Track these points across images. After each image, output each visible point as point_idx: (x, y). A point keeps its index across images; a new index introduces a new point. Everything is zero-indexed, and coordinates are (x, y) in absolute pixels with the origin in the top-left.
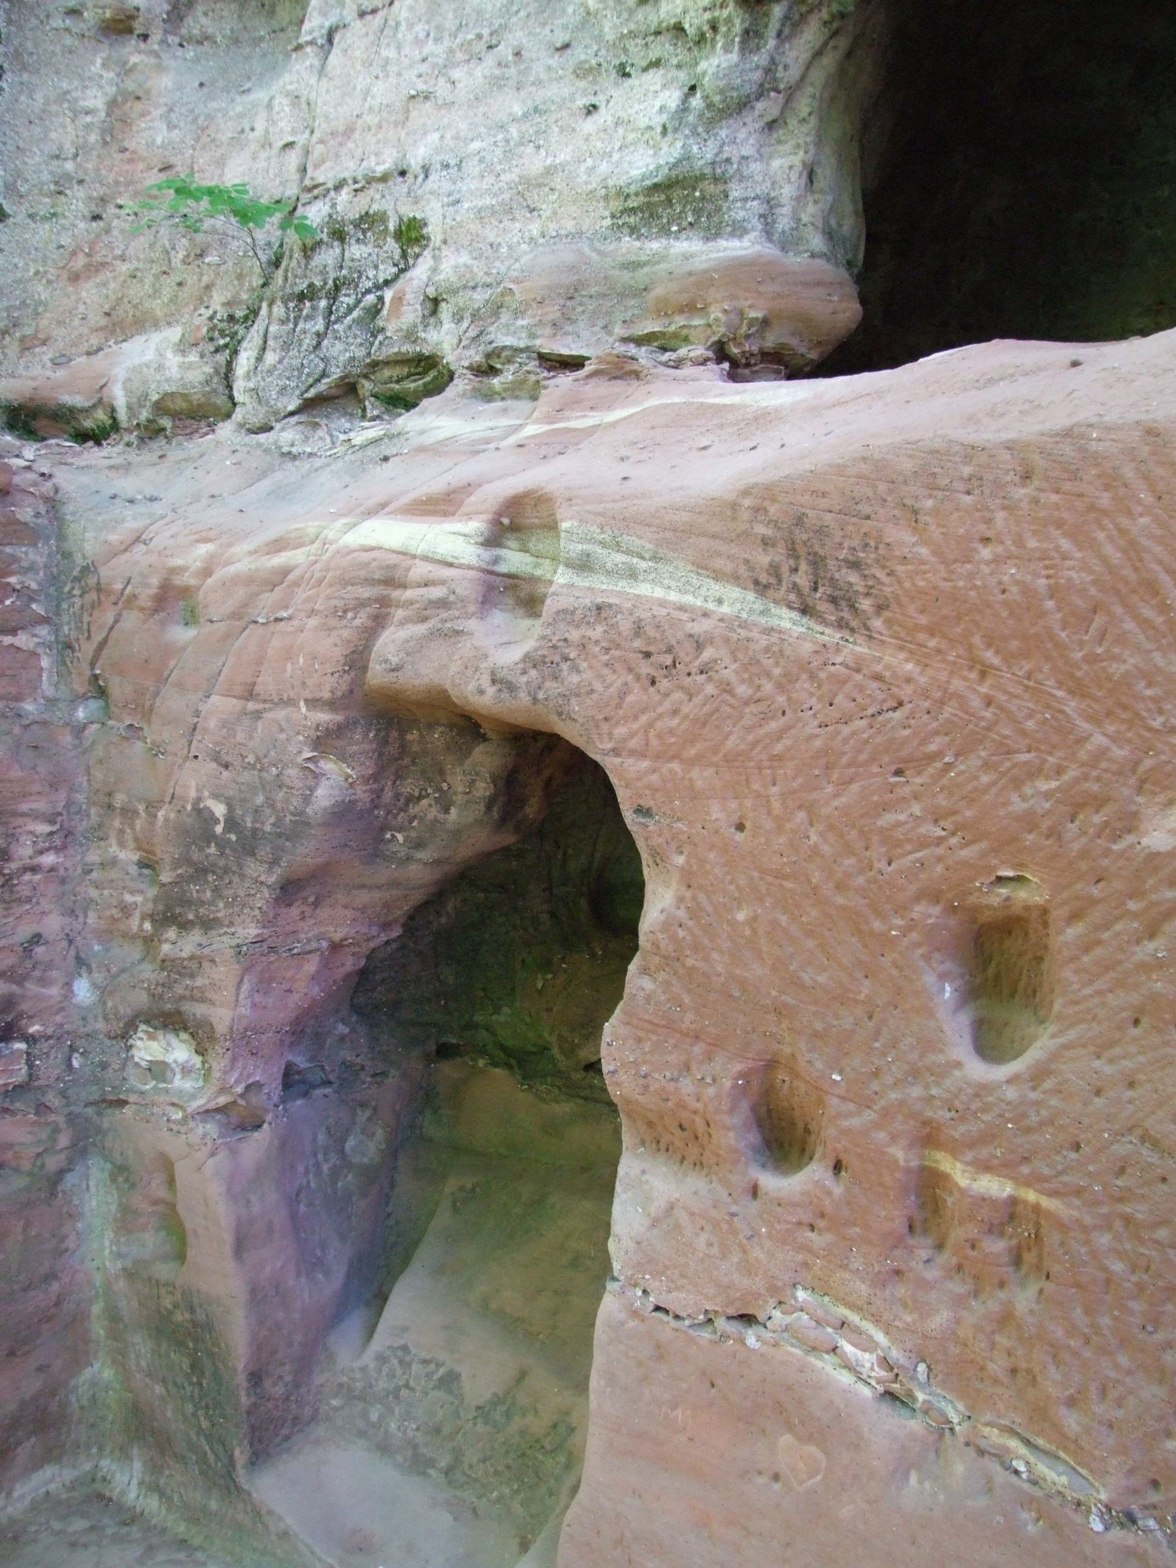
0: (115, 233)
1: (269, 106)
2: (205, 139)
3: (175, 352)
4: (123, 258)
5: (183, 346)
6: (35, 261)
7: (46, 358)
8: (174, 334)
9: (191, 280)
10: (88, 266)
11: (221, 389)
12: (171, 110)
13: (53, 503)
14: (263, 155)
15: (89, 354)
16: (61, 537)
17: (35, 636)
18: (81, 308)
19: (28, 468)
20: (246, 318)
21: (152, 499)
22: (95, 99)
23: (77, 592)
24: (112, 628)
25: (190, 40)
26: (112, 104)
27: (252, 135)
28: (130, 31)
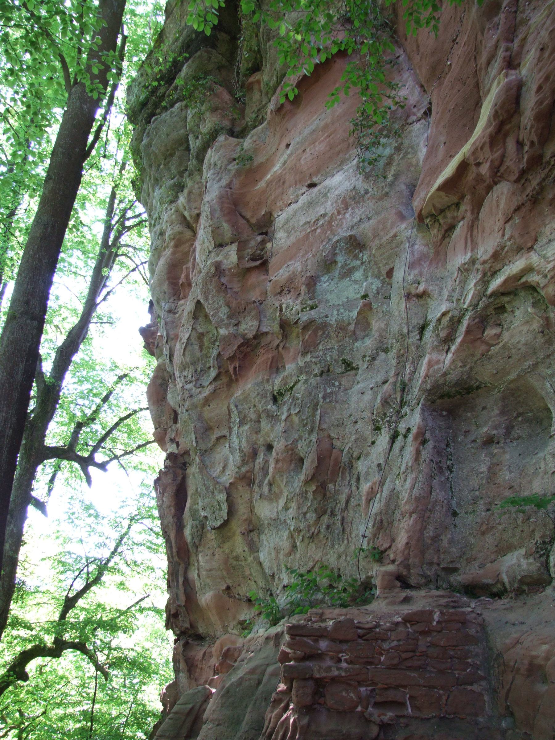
0: (496, 515)
1: (545, 459)
2: (523, 474)
3: (524, 559)
4: (500, 524)
5: (527, 556)
6: (469, 529)
7: (476, 565)
8: (523, 551)
9: (526, 529)
10: (487, 528)
11: (545, 572)
12: (510, 466)
13: (483, 626)
14: (546, 476)
15: (491, 562)
16: (488, 641)
17: (480, 685)
18: (487, 545)
19: (472, 612)
20: (550, 542)
21: (522, 623)
22: (484, 468)
23: (496, 666)
24: (512, 683)
25: (514, 439)
26: (489, 469)
27: (540, 470)
28: (493, 442)
